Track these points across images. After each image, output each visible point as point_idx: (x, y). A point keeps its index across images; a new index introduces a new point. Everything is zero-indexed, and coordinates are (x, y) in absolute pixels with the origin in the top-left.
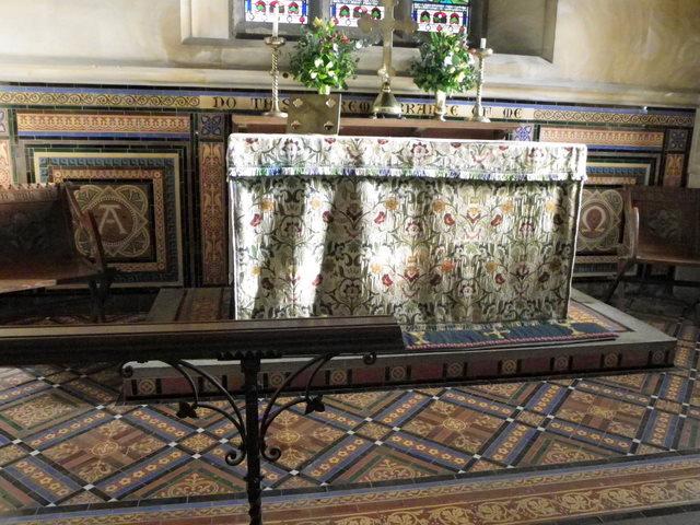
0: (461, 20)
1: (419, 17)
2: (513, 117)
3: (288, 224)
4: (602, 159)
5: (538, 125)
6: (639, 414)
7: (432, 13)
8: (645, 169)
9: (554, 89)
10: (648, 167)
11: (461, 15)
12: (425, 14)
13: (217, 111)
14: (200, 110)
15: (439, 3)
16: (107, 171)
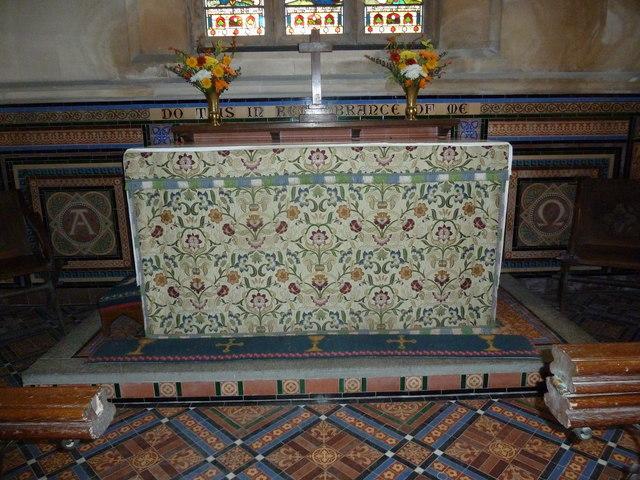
0: (415, 19)
1: (372, 19)
2: (458, 113)
3: (189, 236)
4: (528, 152)
5: (486, 119)
6: (548, 455)
7: (385, 15)
8: (608, 160)
9: (502, 81)
10: (612, 157)
11: (414, 14)
12: (379, 16)
13: (166, 122)
14: (151, 122)
15: (392, 5)
16: (75, 180)
